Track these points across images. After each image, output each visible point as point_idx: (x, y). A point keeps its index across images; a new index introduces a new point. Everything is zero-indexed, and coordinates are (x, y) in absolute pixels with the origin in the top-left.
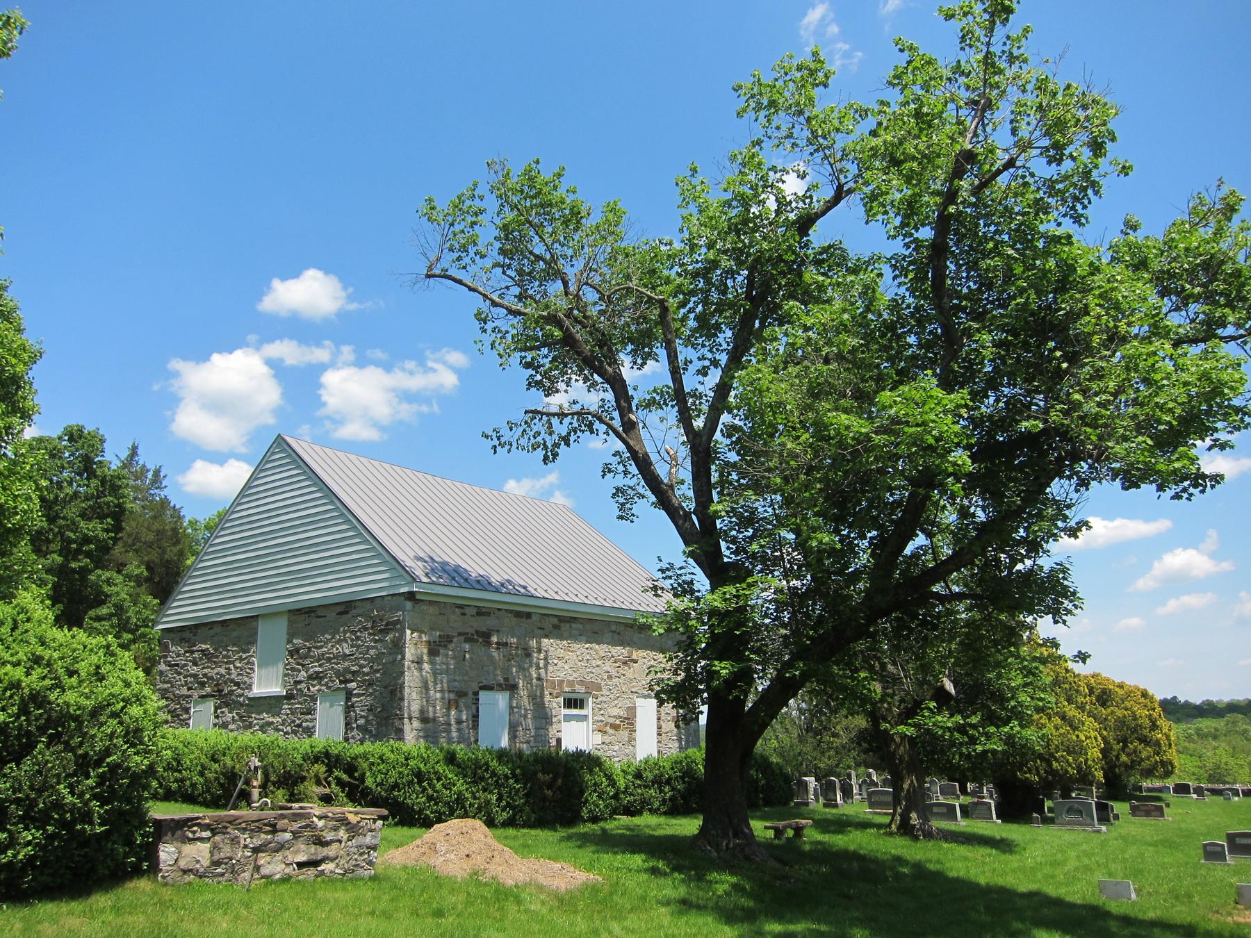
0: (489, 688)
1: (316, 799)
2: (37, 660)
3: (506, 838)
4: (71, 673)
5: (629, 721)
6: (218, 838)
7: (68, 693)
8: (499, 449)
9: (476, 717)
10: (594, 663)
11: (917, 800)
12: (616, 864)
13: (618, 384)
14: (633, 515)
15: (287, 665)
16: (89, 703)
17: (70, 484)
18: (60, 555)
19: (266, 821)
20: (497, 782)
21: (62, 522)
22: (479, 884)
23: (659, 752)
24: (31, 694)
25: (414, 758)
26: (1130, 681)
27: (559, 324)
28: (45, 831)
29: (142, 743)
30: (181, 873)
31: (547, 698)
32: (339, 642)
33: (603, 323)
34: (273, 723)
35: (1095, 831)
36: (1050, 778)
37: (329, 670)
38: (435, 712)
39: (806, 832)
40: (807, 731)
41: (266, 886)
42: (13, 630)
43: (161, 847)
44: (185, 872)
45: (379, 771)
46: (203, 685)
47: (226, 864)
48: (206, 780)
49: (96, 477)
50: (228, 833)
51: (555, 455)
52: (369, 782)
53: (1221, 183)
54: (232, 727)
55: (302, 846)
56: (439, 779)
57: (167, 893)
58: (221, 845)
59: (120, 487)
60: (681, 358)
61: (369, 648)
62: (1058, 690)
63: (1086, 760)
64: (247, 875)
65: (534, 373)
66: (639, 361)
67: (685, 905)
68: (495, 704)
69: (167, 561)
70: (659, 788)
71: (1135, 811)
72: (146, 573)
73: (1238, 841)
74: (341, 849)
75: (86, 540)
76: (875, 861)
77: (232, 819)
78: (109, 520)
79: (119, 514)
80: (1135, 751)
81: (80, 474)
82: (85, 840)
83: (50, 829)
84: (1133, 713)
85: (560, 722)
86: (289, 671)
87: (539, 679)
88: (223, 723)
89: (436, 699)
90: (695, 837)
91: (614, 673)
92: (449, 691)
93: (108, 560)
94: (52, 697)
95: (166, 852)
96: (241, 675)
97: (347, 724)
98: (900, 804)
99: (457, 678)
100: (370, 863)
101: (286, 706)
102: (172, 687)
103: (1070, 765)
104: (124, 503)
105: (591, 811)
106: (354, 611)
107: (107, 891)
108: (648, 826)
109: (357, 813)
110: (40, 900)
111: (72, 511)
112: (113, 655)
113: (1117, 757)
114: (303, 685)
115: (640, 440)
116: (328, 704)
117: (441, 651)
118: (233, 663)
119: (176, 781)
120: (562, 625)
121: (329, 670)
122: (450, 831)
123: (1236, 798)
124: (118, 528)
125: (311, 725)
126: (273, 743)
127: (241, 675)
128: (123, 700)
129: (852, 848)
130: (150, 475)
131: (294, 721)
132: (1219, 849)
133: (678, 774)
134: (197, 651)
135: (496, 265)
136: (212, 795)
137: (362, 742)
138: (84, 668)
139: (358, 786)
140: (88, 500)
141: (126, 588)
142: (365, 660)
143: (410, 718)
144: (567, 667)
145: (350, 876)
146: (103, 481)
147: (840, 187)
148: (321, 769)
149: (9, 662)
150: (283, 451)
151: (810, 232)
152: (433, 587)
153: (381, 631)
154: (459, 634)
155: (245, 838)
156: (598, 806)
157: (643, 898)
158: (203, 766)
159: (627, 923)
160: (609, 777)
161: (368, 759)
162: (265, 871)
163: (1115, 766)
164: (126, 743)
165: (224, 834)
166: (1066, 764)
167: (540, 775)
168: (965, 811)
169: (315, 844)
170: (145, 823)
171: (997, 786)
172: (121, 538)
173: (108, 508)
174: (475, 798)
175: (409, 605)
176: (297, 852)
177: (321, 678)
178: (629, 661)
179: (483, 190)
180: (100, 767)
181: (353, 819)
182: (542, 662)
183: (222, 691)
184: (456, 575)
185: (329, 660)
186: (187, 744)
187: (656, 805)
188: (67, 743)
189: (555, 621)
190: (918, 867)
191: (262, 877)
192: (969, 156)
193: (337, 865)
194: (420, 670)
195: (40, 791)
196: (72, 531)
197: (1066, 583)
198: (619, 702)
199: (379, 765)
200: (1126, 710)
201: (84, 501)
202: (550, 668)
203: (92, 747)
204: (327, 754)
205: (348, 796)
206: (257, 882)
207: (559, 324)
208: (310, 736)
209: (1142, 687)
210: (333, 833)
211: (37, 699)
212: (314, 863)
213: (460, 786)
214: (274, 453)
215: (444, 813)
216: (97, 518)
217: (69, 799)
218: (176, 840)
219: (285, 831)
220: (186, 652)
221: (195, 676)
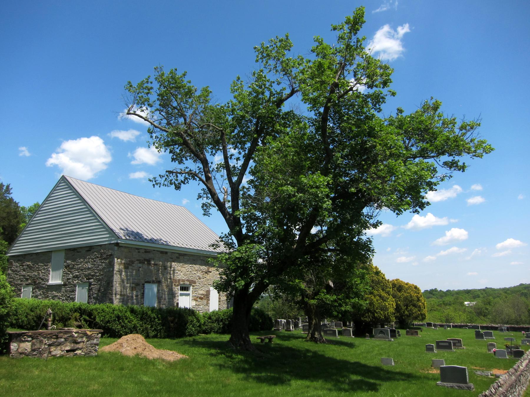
0: (148, 282)
1: (75, 327)
3: (153, 342)
5: (207, 296)
6: (34, 341)
8: (156, 185)
9: (143, 294)
11: (318, 328)
12: (195, 352)
13: (205, 162)
14: (210, 214)
15: (64, 272)
22: (139, 359)
25: (116, 310)
26: (411, 282)
27: (181, 136)
29: (5, 304)
30: (19, 354)
31: (174, 286)
32: (87, 262)
33: (200, 137)
34: (57, 296)
35: (389, 341)
36: (374, 320)
37: (82, 274)
38: (126, 292)
39: (273, 340)
40: (286, 300)
41: (53, 359)
43: (12, 344)
44: (21, 353)
45: (102, 316)
46: (27, 279)
47: (37, 350)
48: (28, 320)
50: (39, 339)
52: (97, 320)
53: (432, 98)
54: (40, 297)
56: (126, 319)
57: (14, 362)
58: (36, 343)
61: (99, 265)
62: (379, 286)
63: (388, 313)
64: (46, 355)
66: (214, 152)
67: (221, 367)
68: (152, 290)
69: (12, 225)
70: (218, 323)
71: (407, 333)
73: (440, 344)
74: (84, 345)
76: (299, 351)
80: (411, 310)
84: (411, 295)
85: (178, 296)
86: (65, 274)
87: (170, 279)
88: (36, 295)
90: (228, 342)
91: (201, 277)
92: (133, 283)
95: (14, 346)
97: (89, 296)
98: (311, 329)
100: (96, 351)
101: (63, 289)
102: (14, 280)
103: (381, 315)
106: (93, 250)
108: (213, 338)
109: (90, 331)
113: (404, 312)
114: (70, 280)
115: (212, 184)
116: (81, 288)
118: (40, 270)
119: (15, 319)
120: (180, 257)
121: (82, 274)
122: (128, 339)
123: (449, 329)
125: (74, 296)
126: (57, 304)
130: (5, 188)
131: (66, 295)
132: (432, 347)
134: (25, 265)
135: (157, 110)
136: (31, 325)
137: (95, 303)
139: (93, 322)
142: (97, 270)
143: (116, 294)
144: (182, 274)
145: (87, 355)
147: (293, 89)
148: (77, 315)
150: (65, 182)
151: (282, 106)
152: (126, 241)
154: (137, 260)
155: (46, 341)
156: (192, 330)
157: (203, 364)
158: (27, 313)
159: (196, 373)
161: (97, 311)
162: (53, 353)
163: (403, 316)
165: (37, 339)
166: (380, 315)
168: (340, 333)
169: (74, 343)
170: (5, 335)
171: (354, 322)
174: (141, 326)
175: (116, 248)
176: (66, 346)
177: (79, 278)
179: (152, 79)
181: (89, 333)
182: (172, 272)
183: (36, 282)
184: (137, 236)
185: (82, 270)
186: (20, 304)
189: (177, 255)
190: (315, 353)
191: (53, 356)
192: (336, 85)
193: (82, 351)
194: (121, 275)
197: (370, 246)
199: (102, 313)
200: (408, 293)
204: (80, 309)
206: (50, 358)
207: (181, 136)
208: (73, 301)
209: (415, 285)
210: (81, 339)
213: (135, 321)
214: (60, 183)
218: (17, 341)
219: (61, 338)
221: (24, 276)
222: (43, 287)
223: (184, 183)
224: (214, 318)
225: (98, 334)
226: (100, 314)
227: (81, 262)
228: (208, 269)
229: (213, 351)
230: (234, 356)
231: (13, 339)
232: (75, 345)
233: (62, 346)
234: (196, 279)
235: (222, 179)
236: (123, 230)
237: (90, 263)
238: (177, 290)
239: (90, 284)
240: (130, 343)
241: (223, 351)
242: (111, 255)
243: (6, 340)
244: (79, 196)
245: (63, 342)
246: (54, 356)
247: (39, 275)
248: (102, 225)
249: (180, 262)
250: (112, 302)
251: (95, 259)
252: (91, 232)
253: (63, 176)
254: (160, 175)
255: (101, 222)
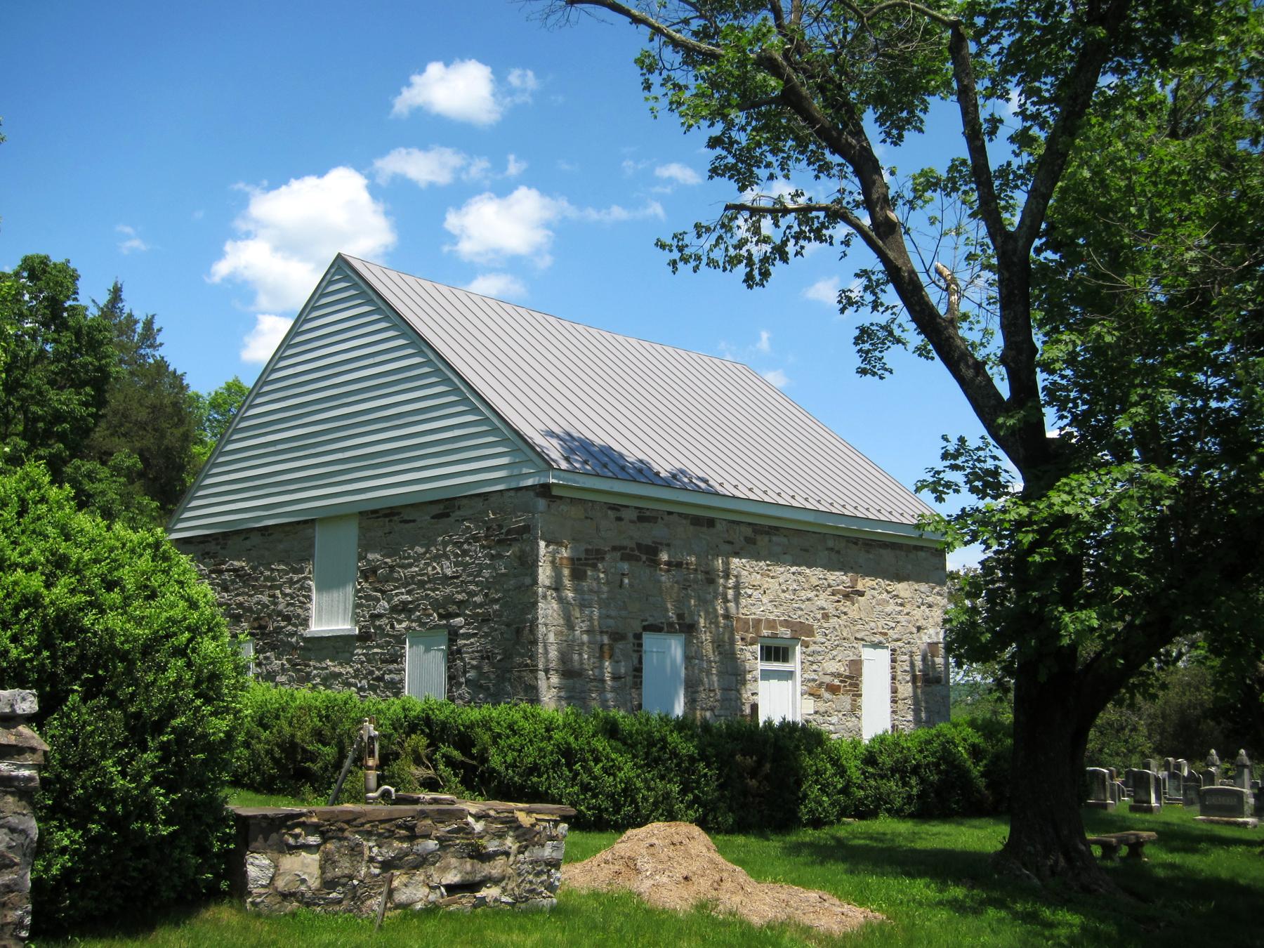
0: (655, 628)
1: (417, 785)
2: (60, 563)
4: (110, 586)
5: (851, 681)
6: (330, 846)
7: (111, 614)
8: (680, 265)
9: (638, 670)
10: (804, 594)
13: (866, 167)
15: (359, 591)
16: (143, 632)
17: (34, 338)
18: (23, 439)
19: (400, 821)
20: (678, 765)
21: (24, 392)
23: (893, 727)
24: (57, 617)
28: (87, 831)
30: (279, 899)
31: (739, 645)
32: (437, 558)
34: (340, 674)
42: (20, 514)
43: (249, 858)
44: (286, 896)
45: (510, 746)
47: (344, 885)
49: (67, 328)
50: (346, 839)
51: (765, 274)
52: (495, 761)
54: (283, 679)
55: (453, 861)
56: (597, 760)
59: (101, 343)
60: (983, 114)
61: (481, 567)
65: (724, 153)
70: (902, 778)
72: (140, 465)
75: (58, 417)
77: (350, 817)
78: (88, 389)
79: (100, 381)
81: (46, 325)
82: (142, 848)
83: (94, 828)
87: (727, 616)
88: (269, 673)
89: (583, 644)
90: (999, 854)
91: (832, 611)
93: (88, 447)
94: (87, 622)
95: (257, 867)
96: (292, 605)
97: (451, 678)
99: (613, 613)
100: (551, 888)
104: (108, 365)
105: (811, 811)
106: (458, 513)
107: (177, 925)
109: (529, 812)
110: (82, 936)
111: (37, 377)
112: (166, 558)
114: (384, 621)
115: (902, 251)
116: (422, 648)
117: (589, 573)
118: (279, 587)
120: (759, 538)
122: (654, 840)
124: (100, 401)
125: (397, 678)
127: (292, 605)
128: (188, 629)
129: (1224, 874)
130: (139, 328)
131: (372, 673)
133: (930, 759)
138: (127, 576)
139: (475, 768)
140: (59, 361)
141: (114, 486)
142: (477, 584)
143: (547, 671)
144: (765, 600)
146: (78, 334)
148: (419, 741)
149: (17, 565)
150: (345, 278)
152: (570, 476)
153: (500, 542)
154: (614, 549)
155: (371, 848)
156: (820, 803)
160: (835, 762)
162: (401, 897)
164: (197, 696)
165: (340, 839)
167: (738, 758)
169: (471, 857)
172: (104, 416)
173: (86, 372)
174: (649, 789)
175: (542, 503)
176: (445, 869)
177: (411, 611)
178: (852, 592)
180: (161, 733)
181: (525, 819)
183: (265, 627)
185: (421, 584)
187: (898, 803)
188: (111, 695)
189: (748, 532)
191: (398, 906)
193: (504, 890)
195: (77, 769)
196: (37, 404)
198: (839, 653)
199: (508, 737)
201: (52, 363)
202: (743, 601)
203: (148, 701)
205: (462, 782)
210: (497, 842)
211: (65, 624)
212: (469, 886)
213: (627, 769)
214: (331, 283)
215: (606, 809)
216: (71, 386)
217: (120, 782)
219: (427, 837)
220: (211, 572)
222: (290, 643)
223: (784, 258)
224: (885, 760)
225: (556, 823)
226: (502, 742)
227: (418, 558)
228: (854, 582)
229: (958, 892)
230: (1047, 913)
231: (256, 840)
232: (478, 865)
233: (432, 870)
234: (815, 619)
235: (935, 231)
236: (558, 437)
237: (448, 558)
238: (751, 656)
239: (453, 635)
240: (663, 856)
241: (996, 894)
242: (526, 529)
243: (228, 843)
244: (398, 321)
245: (432, 852)
246: (404, 906)
247: (276, 604)
248: (486, 420)
249: (758, 558)
250: (534, 700)
251: (466, 546)
252: (449, 448)
253: (339, 256)
254: (697, 226)
255: (481, 413)
